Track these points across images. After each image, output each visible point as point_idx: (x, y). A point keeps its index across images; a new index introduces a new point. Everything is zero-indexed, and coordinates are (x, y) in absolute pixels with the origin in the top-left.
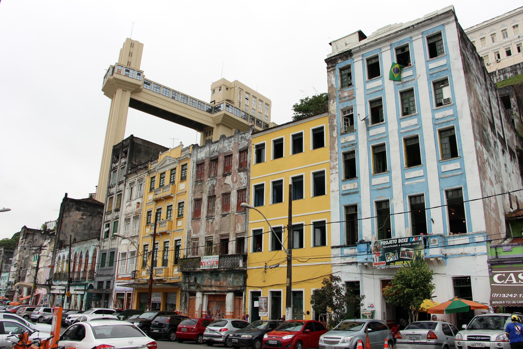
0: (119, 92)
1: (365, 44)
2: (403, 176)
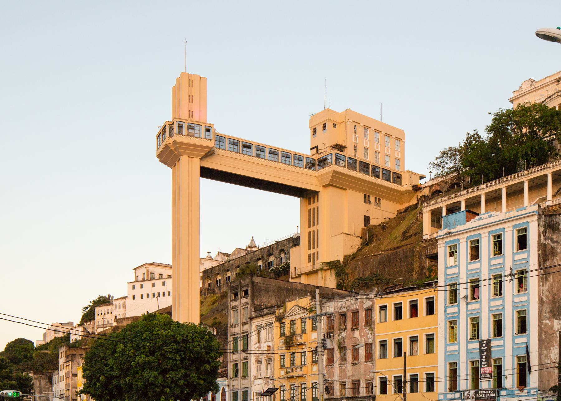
0: (184, 159)
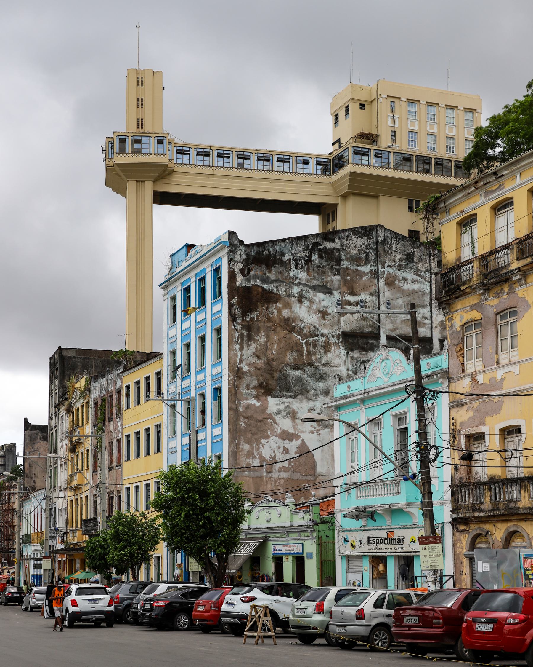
0: (132, 186)
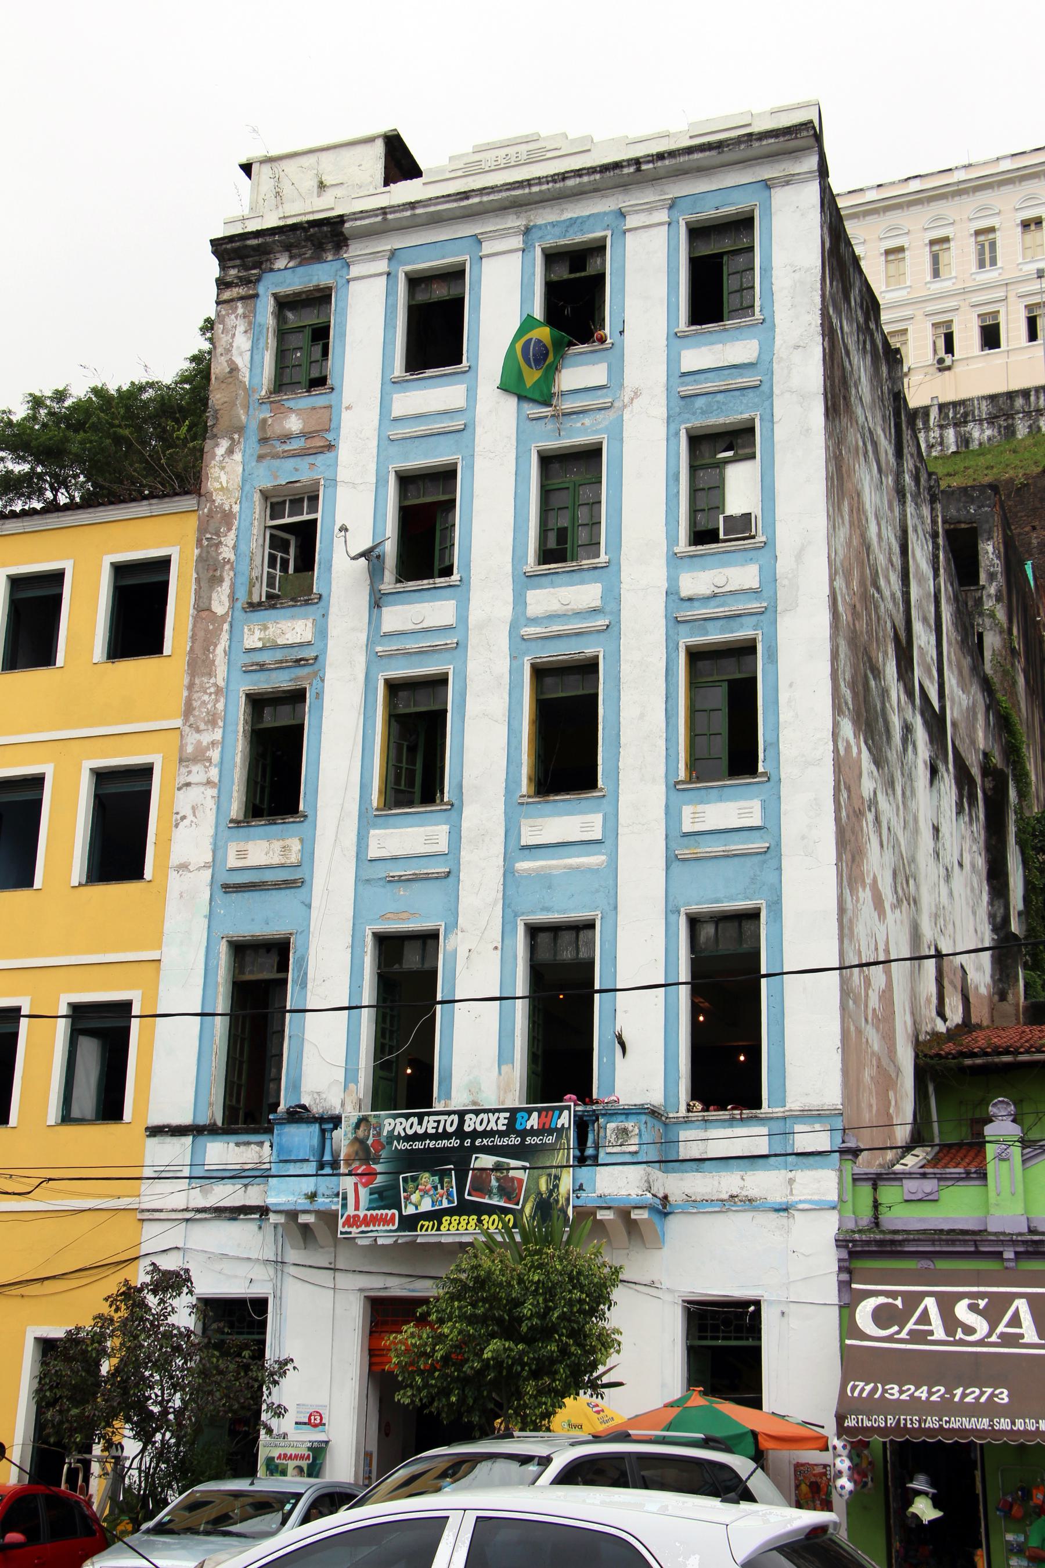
1: (412, 205)
2: (511, 830)
